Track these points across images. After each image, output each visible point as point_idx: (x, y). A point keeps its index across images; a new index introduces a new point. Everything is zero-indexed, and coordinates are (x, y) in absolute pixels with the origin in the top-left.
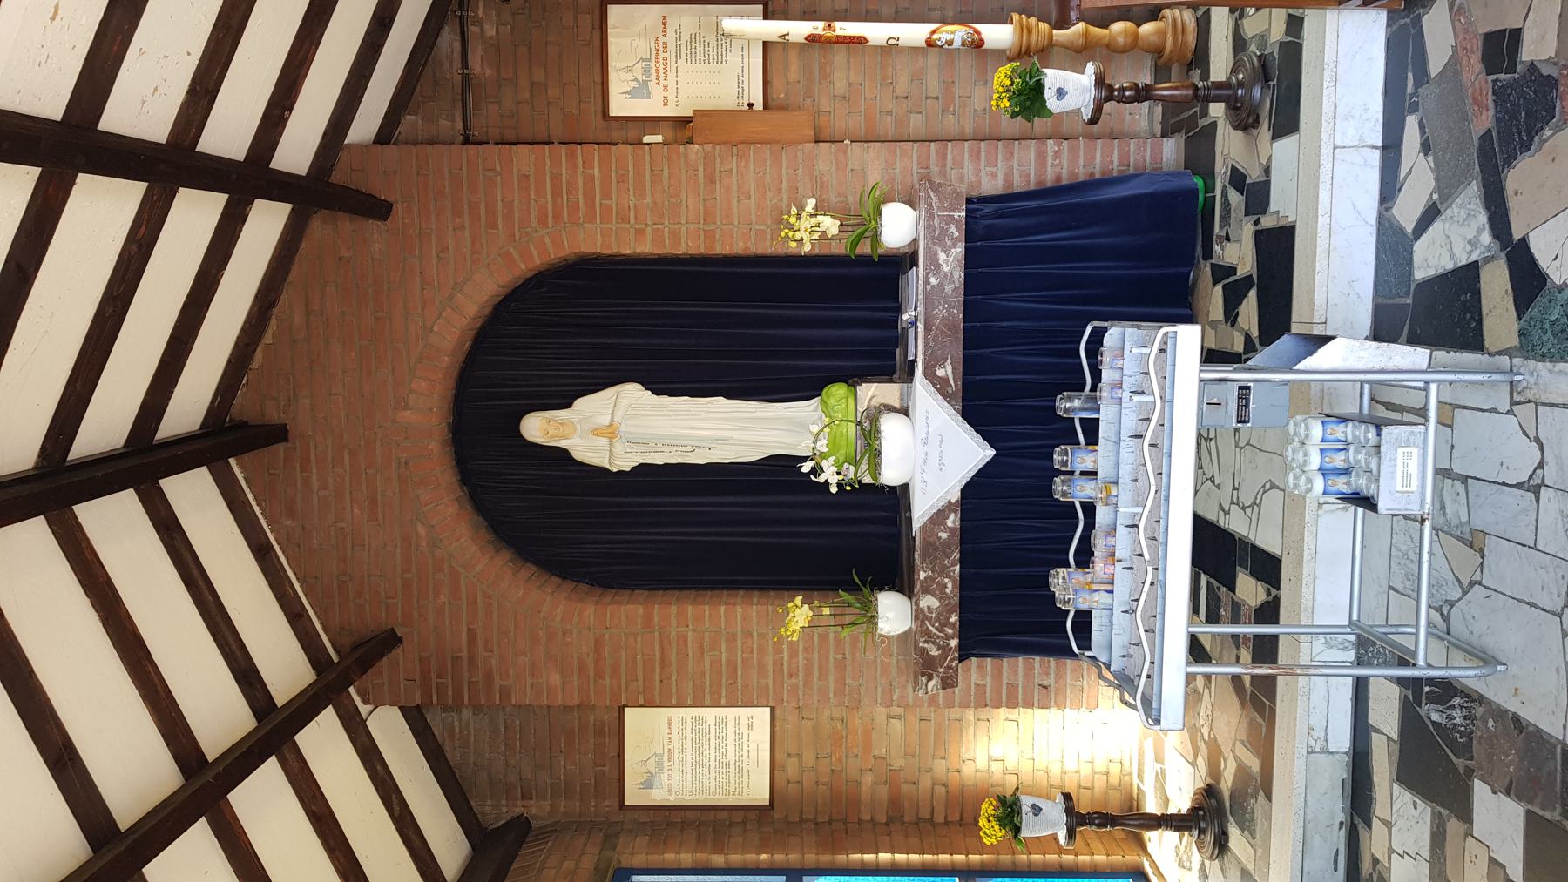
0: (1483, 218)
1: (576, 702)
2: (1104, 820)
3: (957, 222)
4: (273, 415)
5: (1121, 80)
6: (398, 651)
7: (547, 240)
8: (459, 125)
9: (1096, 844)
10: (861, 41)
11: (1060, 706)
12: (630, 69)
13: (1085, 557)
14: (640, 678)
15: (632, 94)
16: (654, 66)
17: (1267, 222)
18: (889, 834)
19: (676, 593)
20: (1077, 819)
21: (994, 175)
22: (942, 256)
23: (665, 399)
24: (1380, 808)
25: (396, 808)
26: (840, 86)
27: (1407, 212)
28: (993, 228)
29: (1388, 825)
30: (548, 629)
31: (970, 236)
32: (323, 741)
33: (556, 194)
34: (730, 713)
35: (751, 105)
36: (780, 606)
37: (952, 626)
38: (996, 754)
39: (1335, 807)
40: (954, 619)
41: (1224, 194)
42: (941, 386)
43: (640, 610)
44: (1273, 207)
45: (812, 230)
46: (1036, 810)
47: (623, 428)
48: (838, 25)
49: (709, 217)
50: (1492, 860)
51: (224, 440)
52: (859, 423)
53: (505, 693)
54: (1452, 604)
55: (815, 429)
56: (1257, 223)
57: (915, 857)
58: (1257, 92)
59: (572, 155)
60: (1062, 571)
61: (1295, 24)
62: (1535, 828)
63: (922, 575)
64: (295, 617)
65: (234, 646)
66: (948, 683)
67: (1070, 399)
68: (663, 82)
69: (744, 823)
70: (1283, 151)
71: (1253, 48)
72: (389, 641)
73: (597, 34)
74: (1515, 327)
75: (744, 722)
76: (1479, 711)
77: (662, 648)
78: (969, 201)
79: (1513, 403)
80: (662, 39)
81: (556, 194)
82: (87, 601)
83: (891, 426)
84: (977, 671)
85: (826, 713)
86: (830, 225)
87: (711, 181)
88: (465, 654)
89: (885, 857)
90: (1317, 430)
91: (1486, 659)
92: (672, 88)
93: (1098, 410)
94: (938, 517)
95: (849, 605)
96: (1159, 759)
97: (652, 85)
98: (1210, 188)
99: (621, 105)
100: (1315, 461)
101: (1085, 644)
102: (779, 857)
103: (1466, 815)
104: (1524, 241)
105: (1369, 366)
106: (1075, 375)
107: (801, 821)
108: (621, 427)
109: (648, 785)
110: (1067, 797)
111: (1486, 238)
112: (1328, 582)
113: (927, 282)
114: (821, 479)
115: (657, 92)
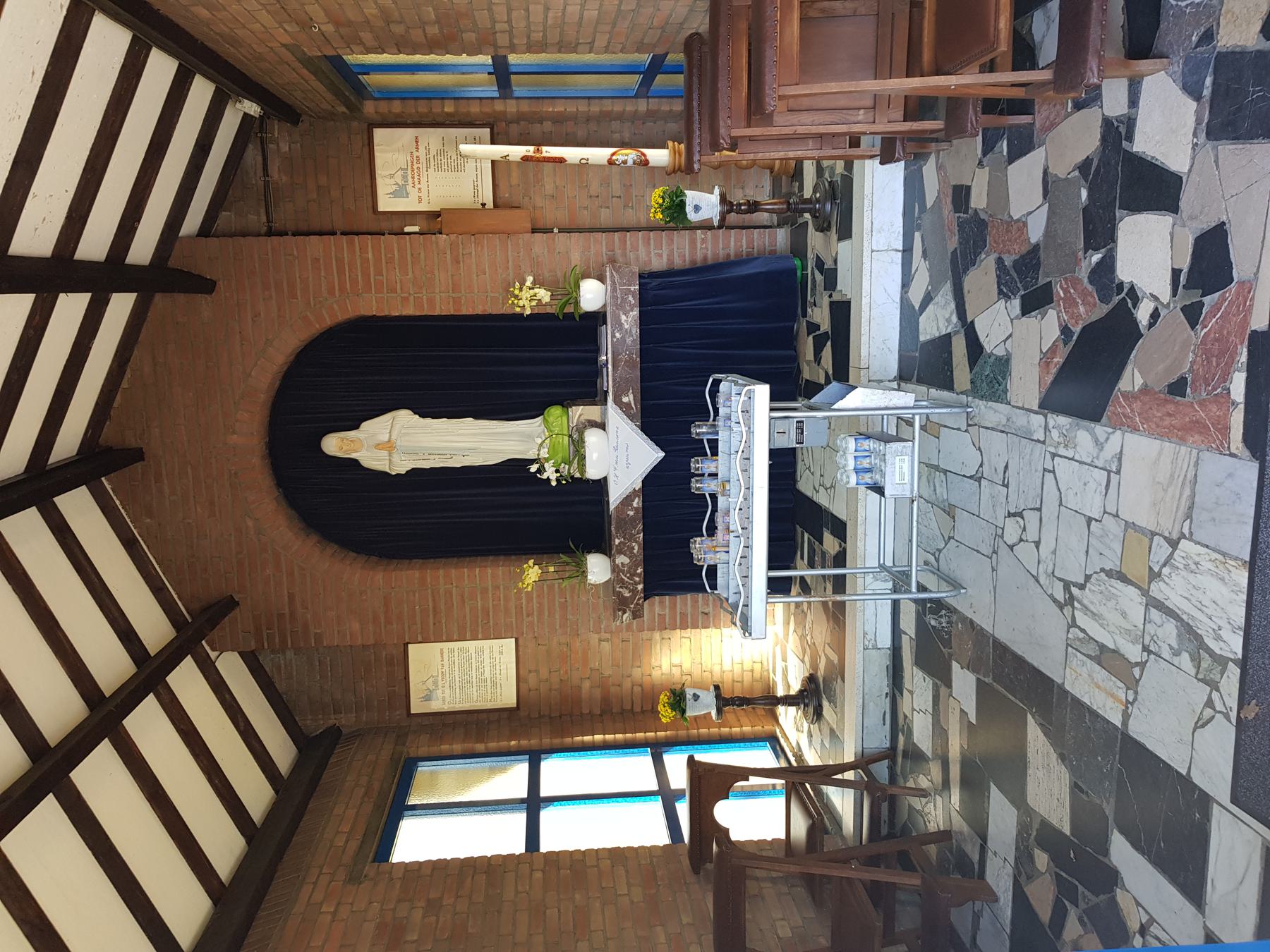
0: (953, 305)
1: (372, 641)
2: (743, 701)
3: (633, 293)
4: (132, 442)
5: (737, 197)
6: (237, 611)
7: (335, 306)
8: (264, 219)
9: (744, 720)
10: (561, 160)
11: (717, 626)
12: (392, 176)
13: (712, 530)
14: (419, 622)
15: (395, 194)
16: (412, 170)
17: (836, 297)
18: (602, 722)
19: (443, 560)
20: (724, 701)
21: (660, 256)
22: (623, 318)
23: (429, 421)
24: (907, 684)
25: (242, 724)
26: (549, 187)
27: (916, 297)
28: (660, 295)
29: (911, 692)
30: (347, 592)
31: (643, 302)
32: (186, 681)
33: (341, 271)
34: (472, 645)
35: (483, 205)
36: (518, 567)
37: (639, 575)
38: (676, 660)
39: (882, 683)
40: (640, 570)
41: (813, 274)
42: (625, 408)
43: (417, 574)
44: (839, 288)
45: (531, 298)
46: (696, 697)
47: (398, 443)
48: (544, 149)
49: (456, 288)
50: (962, 710)
51: (99, 462)
52: (570, 436)
53: (319, 638)
54: (940, 551)
55: (539, 441)
56: (830, 296)
57: (619, 736)
58: (828, 206)
59: (351, 244)
60: (698, 539)
61: (849, 166)
62: (981, 687)
63: (617, 541)
64: (158, 590)
65: (117, 614)
66: (637, 615)
67: (699, 426)
68: (417, 186)
69: (498, 721)
70: (844, 247)
71: (827, 175)
72: (229, 604)
73: (366, 149)
74: (969, 377)
75: (496, 649)
76: (954, 618)
77: (434, 600)
78: (641, 276)
79: (969, 425)
80: (415, 154)
81: (341, 271)
82: (9, 587)
83: (593, 438)
84: (658, 606)
85: (555, 640)
86: (544, 295)
87: (456, 261)
88: (287, 611)
89: (598, 737)
90: (851, 444)
91: (956, 585)
92: (424, 190)
93: (717, 433)
94: (627, 501)
95: (568, 564)
96: (784, 660)
97: (409, 188)
98: (804, 268)
99: (386, 203)
100: (851, 464)
101: (714, 587)
102: (524, 743)
103: (949, 685)
104: (972, 322)
105: (878, 405)
106: (703, 410)
107: (541, 717)
108: (399, 442)
109: (428, 698)
110: (717, 688)
111: (955, 319)
112: (875, 537)
113: (613, 336)
114: (545, 476)
115: (413, 193)
